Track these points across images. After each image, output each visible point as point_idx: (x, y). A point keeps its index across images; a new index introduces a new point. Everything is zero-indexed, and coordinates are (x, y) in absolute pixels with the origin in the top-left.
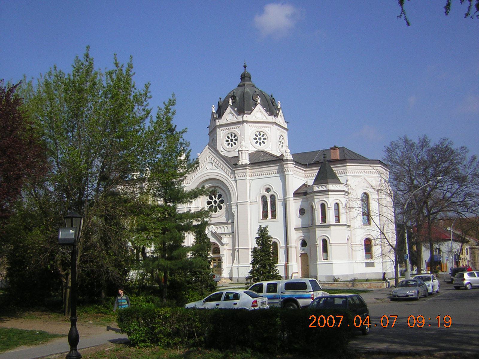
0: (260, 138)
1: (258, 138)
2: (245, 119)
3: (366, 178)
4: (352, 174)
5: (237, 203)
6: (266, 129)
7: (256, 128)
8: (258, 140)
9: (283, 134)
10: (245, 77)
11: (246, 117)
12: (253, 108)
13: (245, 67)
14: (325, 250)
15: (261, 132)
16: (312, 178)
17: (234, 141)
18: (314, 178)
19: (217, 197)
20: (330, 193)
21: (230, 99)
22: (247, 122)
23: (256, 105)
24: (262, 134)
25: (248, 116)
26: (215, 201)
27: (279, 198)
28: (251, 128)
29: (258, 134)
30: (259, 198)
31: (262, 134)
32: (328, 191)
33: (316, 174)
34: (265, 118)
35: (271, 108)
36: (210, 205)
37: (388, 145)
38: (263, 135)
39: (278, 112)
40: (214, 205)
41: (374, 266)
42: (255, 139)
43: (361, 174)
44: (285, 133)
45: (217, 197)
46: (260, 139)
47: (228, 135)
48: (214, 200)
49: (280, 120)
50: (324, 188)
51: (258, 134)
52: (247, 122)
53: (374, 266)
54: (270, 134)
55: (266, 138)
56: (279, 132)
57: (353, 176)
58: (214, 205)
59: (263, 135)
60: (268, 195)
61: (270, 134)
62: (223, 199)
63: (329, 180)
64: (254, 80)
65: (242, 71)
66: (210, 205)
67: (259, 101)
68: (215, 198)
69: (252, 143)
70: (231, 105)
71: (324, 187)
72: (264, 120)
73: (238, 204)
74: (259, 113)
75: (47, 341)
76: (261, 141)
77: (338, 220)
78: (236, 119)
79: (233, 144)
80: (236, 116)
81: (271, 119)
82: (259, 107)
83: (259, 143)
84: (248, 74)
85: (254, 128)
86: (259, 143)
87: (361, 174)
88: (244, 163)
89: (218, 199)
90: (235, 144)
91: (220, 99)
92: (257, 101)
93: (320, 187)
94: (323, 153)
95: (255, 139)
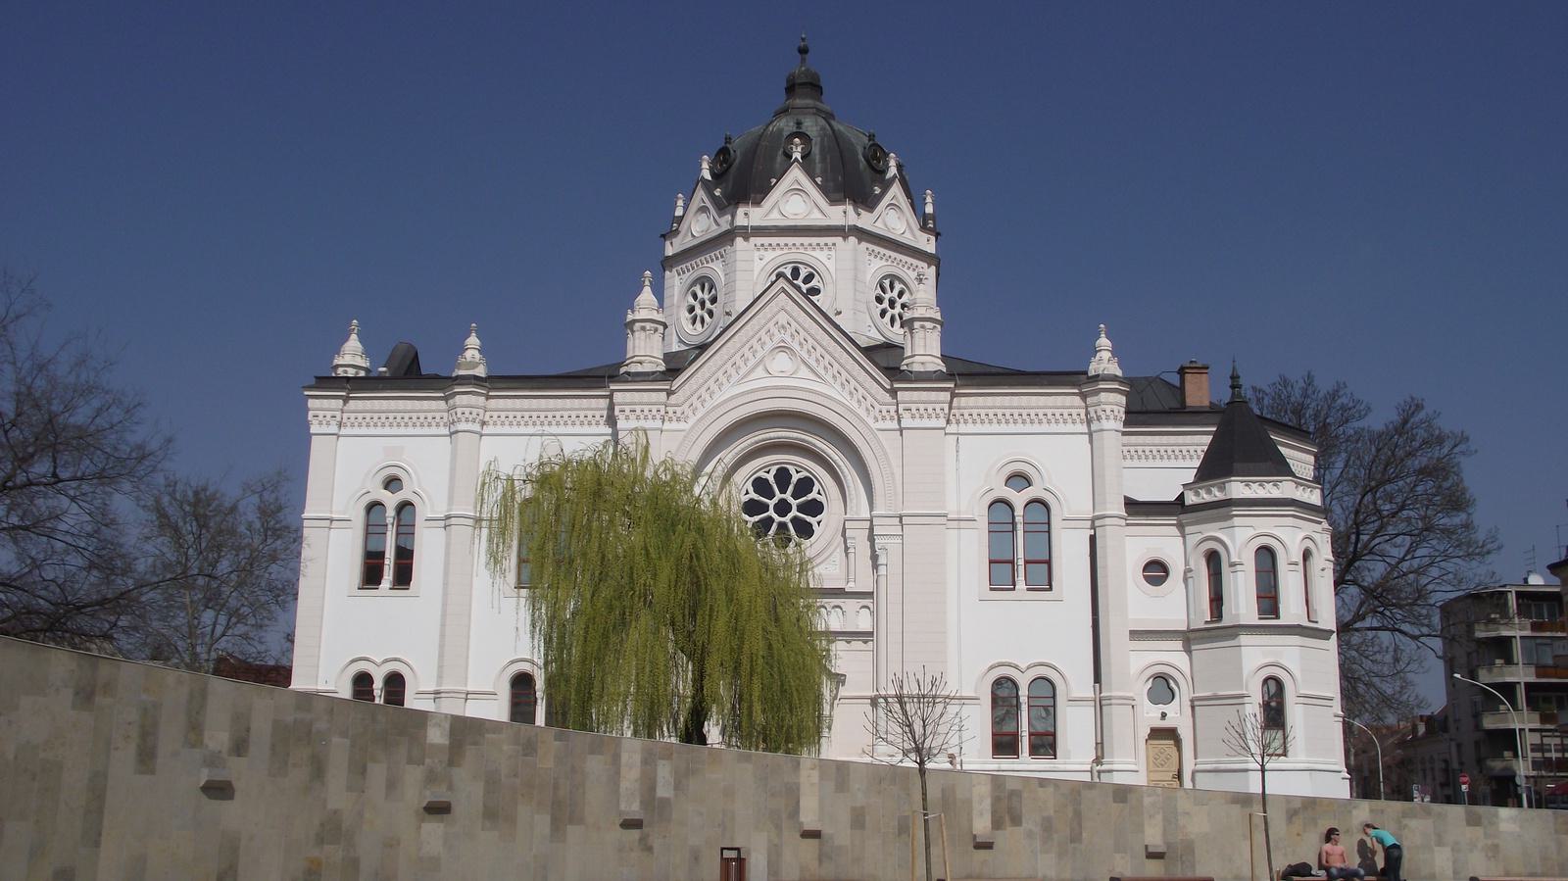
5: (900, 518)
6: (817, 253)
7: (778, 252)
9: (910, 276)
11: (749, 215)
12: (774, 181)
16: (1188, 463)
17: (708, 305)
18: (1197, 463)
19: (791, 488)
22: (749, 233)
26: (783, 502)
28: (762, 252)
32: (1229, 503)
33: (1206, 448)
34: (817, 215)
35: (852, 180)
37: (784, 85)
41: (1152, 730)
45: (791, 488)
49: (894, 217)
50: (1218, 495)
52: (749, 233)
53: (1152, 730)
54: (832, 270)
55: (821, 286)
63: (1237, 466)
68: (783, 491)
71: (1215, 490)
72: (816, 219)
73: (905, 520)
74: (795, 198)
77: (1274, 611)
79: (706, 317)
80: (716, 217)
81: (841, 214)
82: (796, 174)
85: (770, 255)
89: (783, 491)
90: (711, 313)
93: (1203, 492)
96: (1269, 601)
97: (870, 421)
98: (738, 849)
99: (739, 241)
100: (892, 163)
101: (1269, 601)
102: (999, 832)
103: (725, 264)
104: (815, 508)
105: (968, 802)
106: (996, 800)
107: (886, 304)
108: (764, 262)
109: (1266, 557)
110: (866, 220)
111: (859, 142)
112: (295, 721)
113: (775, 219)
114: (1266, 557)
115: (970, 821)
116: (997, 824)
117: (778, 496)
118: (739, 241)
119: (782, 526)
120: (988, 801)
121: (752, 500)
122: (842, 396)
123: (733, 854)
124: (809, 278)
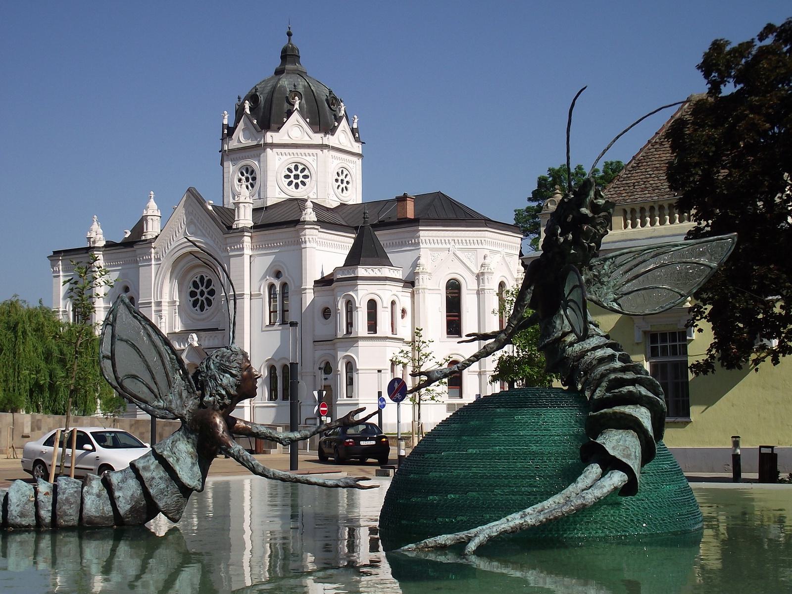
0: (298, 174)
1: (292, 175)
2: (269, 140)
3: (459, 253)
4: (429, 246)
6: (308, 158)
8: (292, 178)
9: (350, 166)
10: (289, 55)
11: (271, 137)
12: (285, 119)
13: (289, 34)
14: (350, 382)
15: (299, 165)
19: (200, 285)
20: (359, 282)
21: (247, 102)
22: (273, 146)
23: (289, 114)
24: (300, 167)
25: (273, 134)
27: (469, 288)
29: (293, 168)
30: (264, 289)
31: (300, 167)
35: (322, 119)
36: (194, 299)
38: (303, 170)
39: (336, 124)
40: (200, 298)
42: (287, 177)
43: (448, 246)
44: (354, 163)
46: (296, 177)
47: (289, 166)
48: (199, 290)
49: (342, 137)
51: (293, 168)
52: (273, 146)
54: (315, 166)
56: (339, 161)
57: (431, 249)
58: (200, 298)
59: (303, 170)
60: (278, 284)
61: (315, 166)
64: (305, 63)
65: (284, 42)
66: (194, 299)
67: (297, 106)
68: (202, 286)
69: (281, 185)
70: (249, 112)
72: (306, 140)
74: (295, 128)
75: (51, 565)
76: (298, 181)
78: (308, 138)
82: (296, 116)
83: (294, 184)
84: (293, 49)
85: (284, 158)
86: (294, 184)
87: (448, 246)
88: (240, 226)
91: (239, 98)
92: (294, 105)
94: (363, 211)
95: (287, 177)
96: (372, 326)
97: (220, 252)
98: (772, 447)
99: (268, 150)
100: (343, 109)
101: (372, 326)
102: (33, 433)
103: (259, 162)
105: (23, 424)
106: (32, 423)
107: (339, 183)
108: (281, 161)
109: (372, 305)
110: (330, 140)
111: (323, 93)
114: (372, 305)
115: (23, 429)
116: (33, 430)
117: (201, 288)
118: (268, 150)
119: (207, 288)
120: (30, 423)
121: (192, 291)
123: (769, 451)
124: (306, 177)
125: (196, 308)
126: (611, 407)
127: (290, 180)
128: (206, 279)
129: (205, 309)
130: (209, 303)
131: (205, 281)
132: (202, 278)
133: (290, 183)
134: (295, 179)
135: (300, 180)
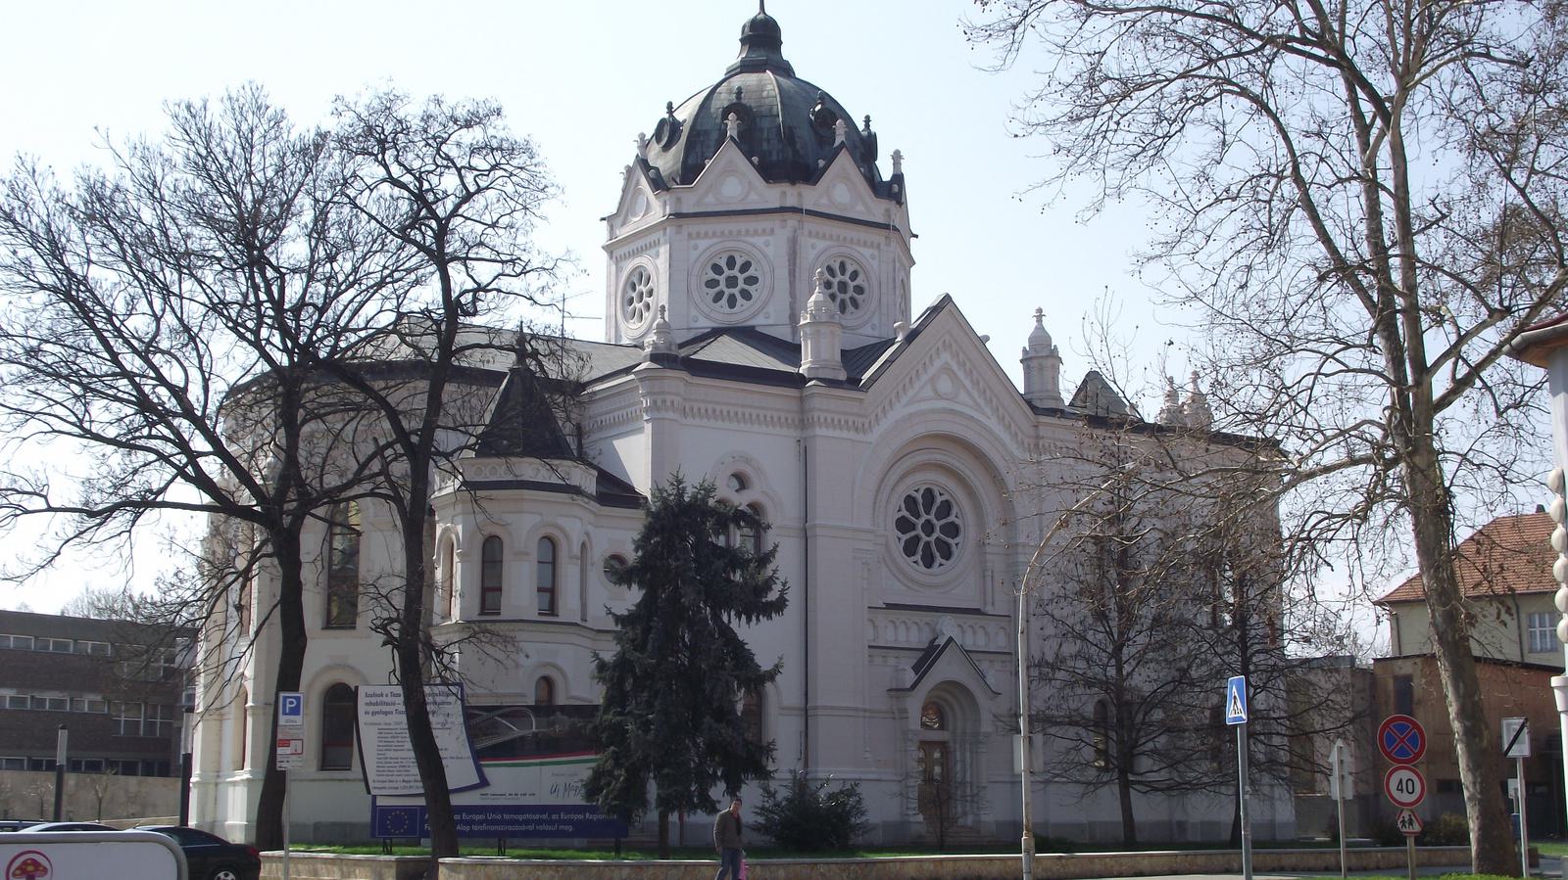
12: (821, 163)
26: (928, 521)
62: (913, 558)
68: (928, 513)
76: (741, 278)
85: (703, 244)
104: (910, 549)
112: (657, 808)
113: (710, 204)
122: (993, 424)
125: (944, 498)
126: (1510, 805)
127: (738, 296)
128: (918, 557)
129: (903, 506)
130: (910, 502)
131: (937, 554)
132: (929, 495)
133: (746, 295)
134: (736, 278)
135: (739, 275)
